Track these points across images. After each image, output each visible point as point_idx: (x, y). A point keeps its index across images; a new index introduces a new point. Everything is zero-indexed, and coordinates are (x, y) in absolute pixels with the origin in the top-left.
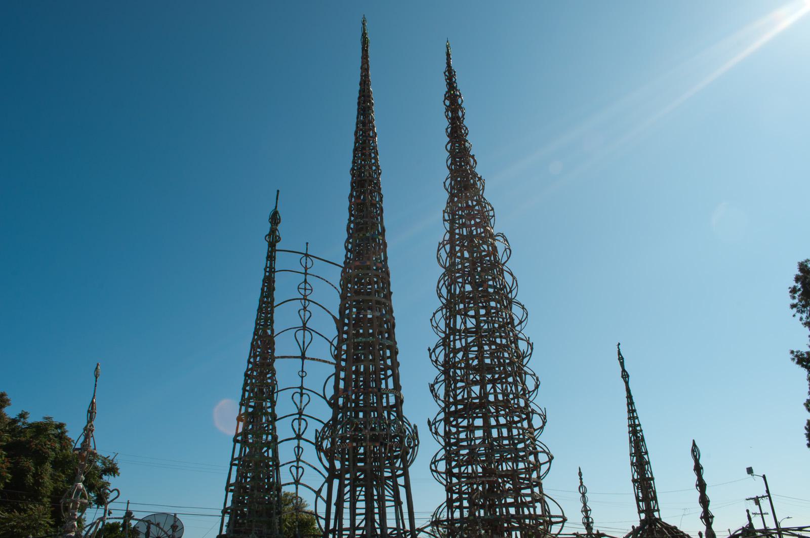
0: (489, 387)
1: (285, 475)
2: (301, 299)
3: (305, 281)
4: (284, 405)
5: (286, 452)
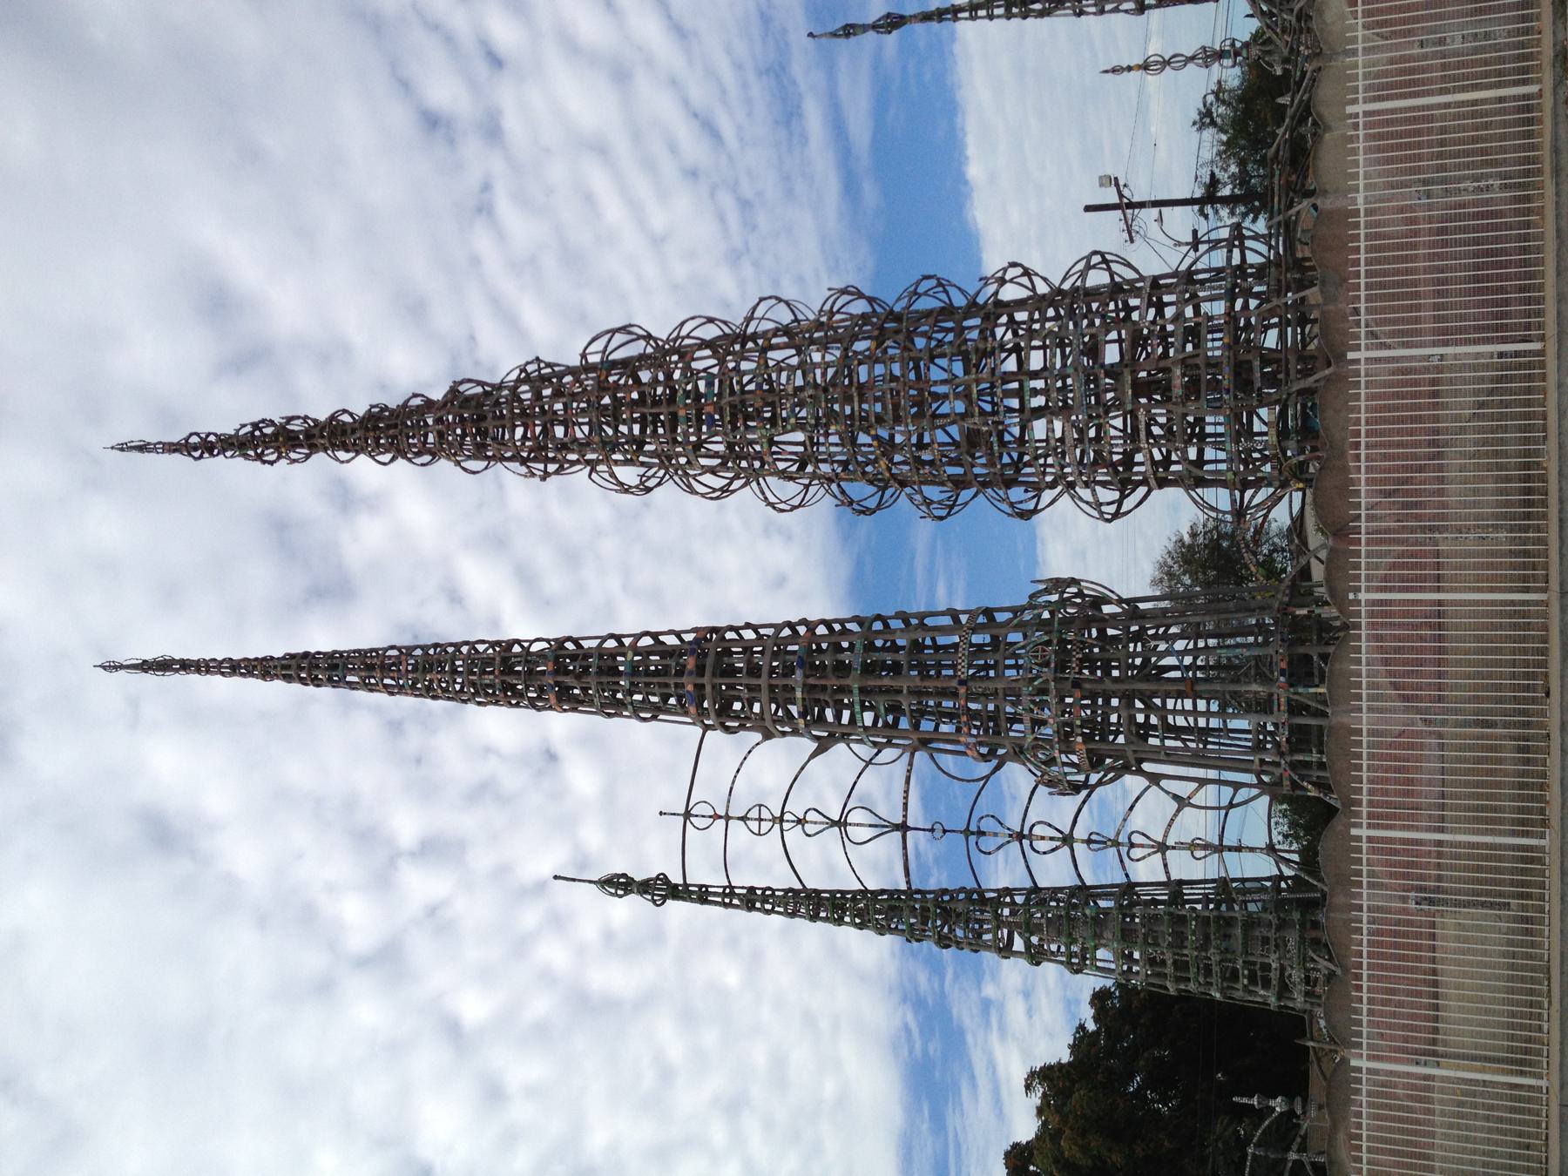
1: (1147, 870)
3: (744, 819)
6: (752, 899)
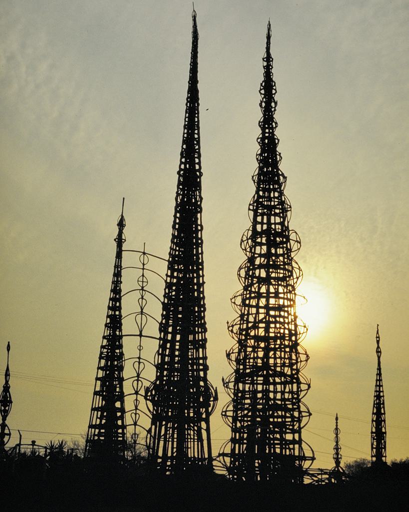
0: (271, 353)
1: (128, 420)
2: (140, 290)
3: (143, 276)
4: (128, 372)
5: (129, 403)
6: (117, 274)
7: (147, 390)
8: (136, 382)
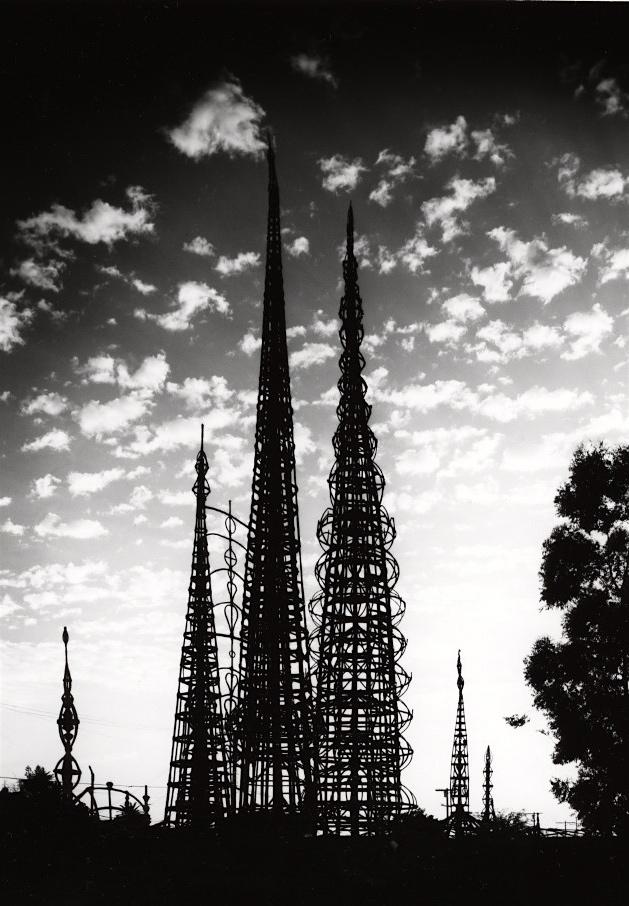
7: (482, 185)
8: (228, 702)
